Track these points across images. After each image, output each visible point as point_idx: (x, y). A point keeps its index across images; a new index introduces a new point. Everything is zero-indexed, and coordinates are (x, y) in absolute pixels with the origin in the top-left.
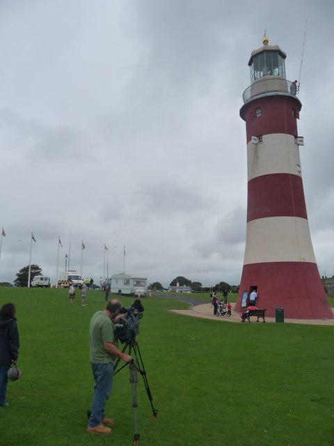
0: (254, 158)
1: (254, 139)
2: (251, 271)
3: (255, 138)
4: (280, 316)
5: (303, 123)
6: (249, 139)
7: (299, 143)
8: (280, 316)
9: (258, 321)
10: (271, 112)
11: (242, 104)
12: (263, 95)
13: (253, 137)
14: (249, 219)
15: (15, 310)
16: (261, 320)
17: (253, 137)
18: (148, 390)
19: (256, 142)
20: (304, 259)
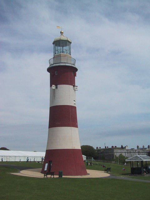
0: (53, 94)
1: (54, 87)
2: (82, 147)
3: (54, 86)
4: (60, 175)
5: (78, 79)
6: (51, 86)
7: (75, 89)
8: (60, 175)
9: (51, 177)
10: (62, 74)
11: (48, 66)
12: (64, 64)
13: (53, 86)
14: (49, 127)
15: (87, 146)
16: (52, 176)
17: (53, 86)
18: (124, 174)
19: (54, 88)
20: (74, 147)
